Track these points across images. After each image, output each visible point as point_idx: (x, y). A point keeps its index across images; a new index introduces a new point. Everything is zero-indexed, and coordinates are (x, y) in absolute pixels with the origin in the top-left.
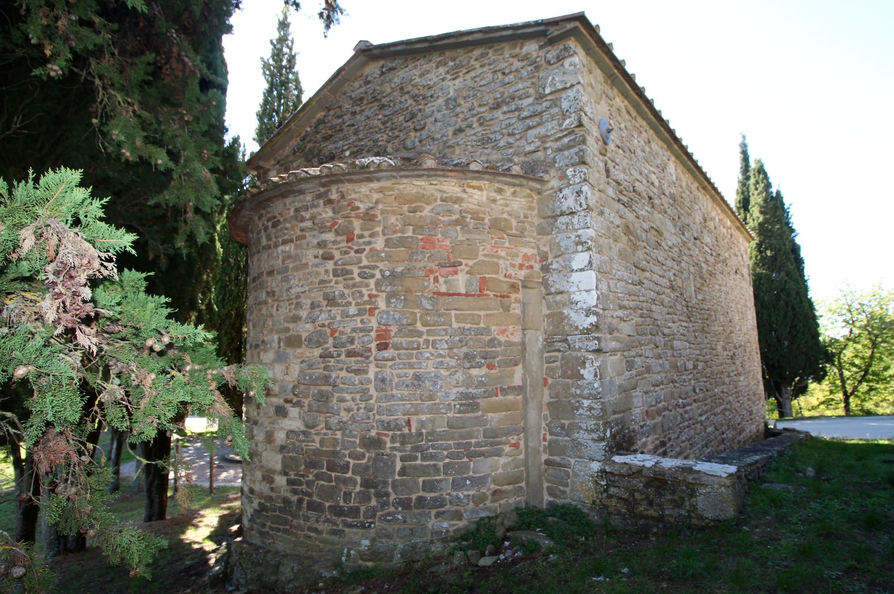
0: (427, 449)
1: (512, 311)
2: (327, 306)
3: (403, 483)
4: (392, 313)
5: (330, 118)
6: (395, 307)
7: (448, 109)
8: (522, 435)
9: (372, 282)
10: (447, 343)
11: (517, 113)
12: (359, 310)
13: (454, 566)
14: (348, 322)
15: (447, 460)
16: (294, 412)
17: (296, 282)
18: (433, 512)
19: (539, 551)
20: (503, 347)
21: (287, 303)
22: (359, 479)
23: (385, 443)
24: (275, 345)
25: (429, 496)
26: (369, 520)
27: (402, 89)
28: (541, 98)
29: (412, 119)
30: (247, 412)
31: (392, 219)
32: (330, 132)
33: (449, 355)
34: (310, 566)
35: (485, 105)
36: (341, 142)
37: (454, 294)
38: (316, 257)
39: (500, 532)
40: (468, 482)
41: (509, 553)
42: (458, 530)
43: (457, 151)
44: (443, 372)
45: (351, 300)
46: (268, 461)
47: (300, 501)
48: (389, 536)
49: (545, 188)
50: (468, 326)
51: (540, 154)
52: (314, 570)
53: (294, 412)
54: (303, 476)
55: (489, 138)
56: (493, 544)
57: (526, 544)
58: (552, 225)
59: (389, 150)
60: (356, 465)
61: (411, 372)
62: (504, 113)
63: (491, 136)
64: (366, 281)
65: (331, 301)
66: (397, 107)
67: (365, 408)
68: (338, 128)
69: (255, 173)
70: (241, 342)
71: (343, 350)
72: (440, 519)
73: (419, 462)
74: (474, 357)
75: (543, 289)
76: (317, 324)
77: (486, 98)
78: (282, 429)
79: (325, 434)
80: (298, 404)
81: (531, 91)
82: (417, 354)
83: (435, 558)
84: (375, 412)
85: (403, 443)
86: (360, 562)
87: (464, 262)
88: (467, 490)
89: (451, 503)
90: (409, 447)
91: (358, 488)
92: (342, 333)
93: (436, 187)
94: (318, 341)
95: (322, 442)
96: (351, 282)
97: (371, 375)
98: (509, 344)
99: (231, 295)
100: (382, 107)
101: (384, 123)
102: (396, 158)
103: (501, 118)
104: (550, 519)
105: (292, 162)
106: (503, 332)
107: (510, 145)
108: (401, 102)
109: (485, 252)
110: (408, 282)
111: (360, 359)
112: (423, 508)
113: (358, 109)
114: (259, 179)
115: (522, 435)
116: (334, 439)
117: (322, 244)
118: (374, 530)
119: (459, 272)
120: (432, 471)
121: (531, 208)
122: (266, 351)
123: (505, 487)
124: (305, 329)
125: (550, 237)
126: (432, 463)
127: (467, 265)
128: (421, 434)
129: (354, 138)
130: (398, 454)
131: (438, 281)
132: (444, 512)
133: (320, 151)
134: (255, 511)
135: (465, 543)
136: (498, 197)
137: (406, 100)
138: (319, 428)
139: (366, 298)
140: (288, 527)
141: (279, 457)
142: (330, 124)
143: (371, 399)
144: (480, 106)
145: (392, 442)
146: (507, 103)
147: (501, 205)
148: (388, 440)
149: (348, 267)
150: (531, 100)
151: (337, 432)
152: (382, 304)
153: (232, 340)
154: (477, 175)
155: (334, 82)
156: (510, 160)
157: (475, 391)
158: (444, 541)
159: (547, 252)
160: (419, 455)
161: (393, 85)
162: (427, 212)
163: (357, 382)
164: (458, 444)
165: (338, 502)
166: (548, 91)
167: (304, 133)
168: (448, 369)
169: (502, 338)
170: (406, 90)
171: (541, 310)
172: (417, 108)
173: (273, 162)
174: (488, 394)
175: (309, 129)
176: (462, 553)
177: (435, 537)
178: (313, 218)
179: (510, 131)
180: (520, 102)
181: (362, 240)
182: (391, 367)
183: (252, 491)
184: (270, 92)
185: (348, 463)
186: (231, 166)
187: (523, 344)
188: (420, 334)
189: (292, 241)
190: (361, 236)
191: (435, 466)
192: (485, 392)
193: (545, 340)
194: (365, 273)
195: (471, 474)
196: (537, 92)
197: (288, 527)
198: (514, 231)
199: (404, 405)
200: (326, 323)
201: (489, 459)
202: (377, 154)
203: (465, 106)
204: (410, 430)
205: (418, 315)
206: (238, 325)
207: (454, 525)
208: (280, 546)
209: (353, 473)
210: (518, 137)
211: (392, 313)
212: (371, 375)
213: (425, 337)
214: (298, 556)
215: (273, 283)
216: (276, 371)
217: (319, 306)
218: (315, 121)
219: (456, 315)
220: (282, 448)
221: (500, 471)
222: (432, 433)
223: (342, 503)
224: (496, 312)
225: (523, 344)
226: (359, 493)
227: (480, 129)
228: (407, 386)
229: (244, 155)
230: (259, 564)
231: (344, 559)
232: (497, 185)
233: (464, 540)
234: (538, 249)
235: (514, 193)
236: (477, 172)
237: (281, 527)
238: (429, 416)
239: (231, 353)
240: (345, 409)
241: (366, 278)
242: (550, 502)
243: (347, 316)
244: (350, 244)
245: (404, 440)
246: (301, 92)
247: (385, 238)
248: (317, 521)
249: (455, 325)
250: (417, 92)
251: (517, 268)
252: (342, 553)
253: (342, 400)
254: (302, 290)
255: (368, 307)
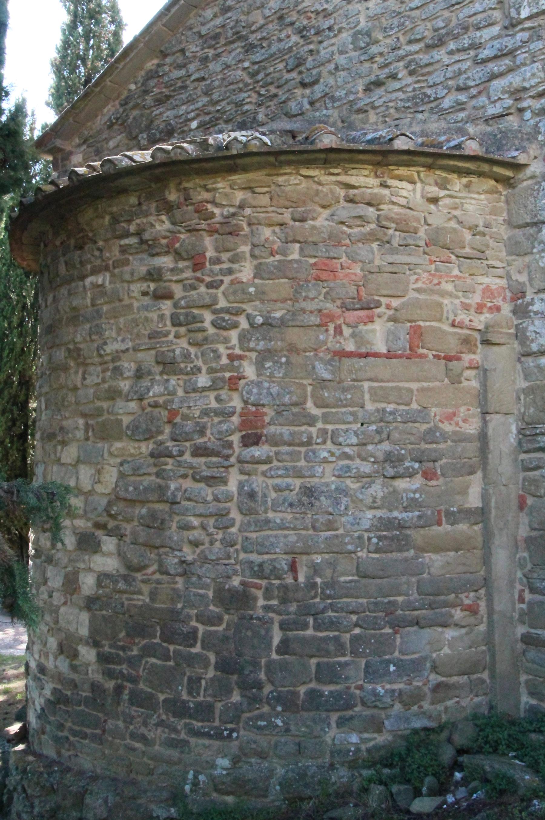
0: (323, 611)
1: (465, 383)
2: (161, 373)
3: (284, 667)
4: (266, 385)
5: (167, 68)
6: (271, 376)
7: (356, 48)
8: (482, 592)
9: (234, 335)
10: (357, 436)
11: (472, 53)
12: (214, 381)
13: (370, 811)
14: (197, 398)
15: (357, 631)
16: (109, 544)
17: (114, 335)
18: (334, 717)
19: (515, 792)
20: (449, 443)
21: (99, 369)
22: (212, 658)
23: (255, 599)
24: (80, 434)
25: (327, 689)
26: (229, 726)
27: (281, 18)
28: (513, 26)
29: (298, 66)
30: (36, 541)
31: (267, 232)
32: (166, 91)
33: (359, 456)
34: (134, 798)
35: (418, 41)
36: (184, 107)
37: (367, 355)
38: (145, 294)
39: (447, 754)
40: (392, 668)
41: (462, 792)
42: (377, 748)
43: (372, 117)
44: (352, 485)
45: (200, 363)
46: (69, 622)
47: (119, 689)
48: (262, 755)
49: (521, 176)
50: (390, 407)
51: (513, 121)
52: (140, 805)
53: (109, 544)
54: (123, 648)
55: (425, 94)
56: (433, 775)
57: (489, 777)
58: (533, 239)
59: (261, 117)
60: (208, 635)
61: (297, 483)
62: (451, 53)
63: (429, 91)
64: (225, 333)
65: (168, 365)
66: (274, 49)
67: (222, 541)
68: (179, 84)
69: (50, 158)
70: (26, 426)
71: (188, 444)
72: (346, 729)
73: (310, 632)
74: (401, 459)
75: (516, 344)
76: (146, 402)
77: (420, 29)
78: (90, 570)
79: (158, 582)
80: (116, 533)
81: (497, 15)
82: (306, 454)
83: (337, 794)
84: (238, 547)
85: (284, 601)
86: (215, 795)
87: (384, 301)
88: (390, 683)
89: (364, 703)
90: (293, 607)
91: (211, 673)
92: (185, 418)
93: (339, 178)
94: (148, 430)
95: (153, 595)
96: (199, 336)
97: (232, 487)
98: (460, 438)
99: (11, 351)
100: (249, 48)
101: (253, 75)
102: (272, 132)
103: (446, 60)
104: (533, 736)
105: (107, 140)
106: (450, 417)
107: (460, 106)
108: (280, 40)
109: (419, 285)
110: (293, 335)
111: (215, 459)
112: (317, 709)
113: (211, 52)
114: (55, 168)
115: (482, 592)
116: (174, 589)
117: (155, 275)
118: (236, 743)
119: (376, 319)
120: (332, 648)
121: (494, 212)
122: (64, 443)
123: (455, 679)
124: (126, 411)
125: (527, 259)
126: (331, 634)
127: (388, 307)
128: (314, 585)
129: (205, 99)
130: (277, 618)
131: (341, 333)
132: (352, 718)
133: (152, 121)
134: (48, 701)
135: (386, 771)
136: (442, 193)
137: (288, 37)
138: (150, 570)
139: (225, 361)
140: (98, 731)
141: (85, 617)
142: (166, 79)
143: (233, 525)
144: (410, 42)
145: (266, 598)
146: (456, 37)
147: (445, 206)
148: (259, 594)
149: (196, 311)
150: (496, 30)
151: (178, 579)
152: (249, 371)
153: (14, 421)
154: (405, 157)
155: (173, 10)
156: (461, 131)
157: (404, 515)
158: (353, 765)
159: (523, 284)
160: (311, 620)
161: (267, 13)
162: (322, 220)
163: (210, 498)
164: (376, 604)
165: (179, 693)
166: (524, 14)
167: (125, 93)
168: (359, 477)
169: (447, 427)
170: (288, 20)
171: (514, 381)
172: (306, 48)
173: (77, 141)
174: (424, 523)
175: (133, 87)
176: (381, 788)
177: (337, 759)
178: (139, 234)
179: (461, 82)
180: (478, 34)
181: (217, 267)
182: (264, 474)
183: (42, 669)
184: (72, 26)
185: (195, 631)
186: (13, 151)
187: (483, 437)
188: (311, 421)
189: (107, 268)
190: (217, 261)
191: (336, 639)
192: (420, 517)
193: (520, 431)
194: (223, 320)
195: (397, 654)
196: (507, 16)
197: (98, 731)
198: (467, 251)
199: (286, 536)
200: (161, 400)
201: (428, 630)
202: (242, 126)
203: (385, 43)
204: (296, 579)
205: (309, 389)
206: (22, 398)
207: (370, 740)
208: (86, 763)
209: (203, 648)
210: (474, 91)
211: (266, 385)
212: (232, 487)
213: (320, 425)
214: (114, 779)
215: (79, 335)
216: (82, 477)
217: (149, 373)
218: (143, 73)
219: (371, 388)
220: (90, 603)
221: (447, 650)
222: (331, 584)
223: (185, 696)
224: (438, 384)
225: (483, 437)
226: (212, 679)
227: (410, 80)
228: (291, 505)
229: (32, 130)
230: (53, 790)
231: (187, 788)
232: (438, 172)
233: (386, 766)
234: (509, 277)
235: (467, 186)
236: (408, 152)
237: (88, 731)
238: (327, 556)
239: (12, 442)
240: (190, 542)
241: (225, 329)
242: (532, 706)
243: (195, 390)
244: (198, 274)
245: (286, 595)
246: (120, 26)
247: (255, 262)
248: (145, 724)
249: (370, 406)
250: (305, 22)
251: (472, 311)
252: (185, 779)
253: (187, 527)
254: (123, 347)
255: (228, 375)
